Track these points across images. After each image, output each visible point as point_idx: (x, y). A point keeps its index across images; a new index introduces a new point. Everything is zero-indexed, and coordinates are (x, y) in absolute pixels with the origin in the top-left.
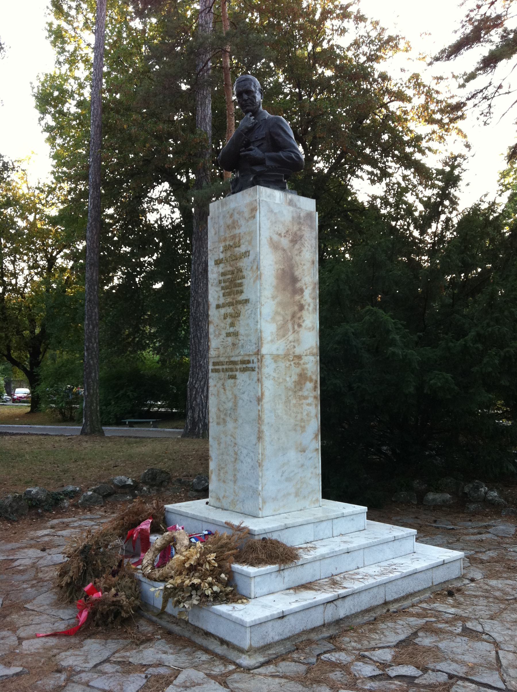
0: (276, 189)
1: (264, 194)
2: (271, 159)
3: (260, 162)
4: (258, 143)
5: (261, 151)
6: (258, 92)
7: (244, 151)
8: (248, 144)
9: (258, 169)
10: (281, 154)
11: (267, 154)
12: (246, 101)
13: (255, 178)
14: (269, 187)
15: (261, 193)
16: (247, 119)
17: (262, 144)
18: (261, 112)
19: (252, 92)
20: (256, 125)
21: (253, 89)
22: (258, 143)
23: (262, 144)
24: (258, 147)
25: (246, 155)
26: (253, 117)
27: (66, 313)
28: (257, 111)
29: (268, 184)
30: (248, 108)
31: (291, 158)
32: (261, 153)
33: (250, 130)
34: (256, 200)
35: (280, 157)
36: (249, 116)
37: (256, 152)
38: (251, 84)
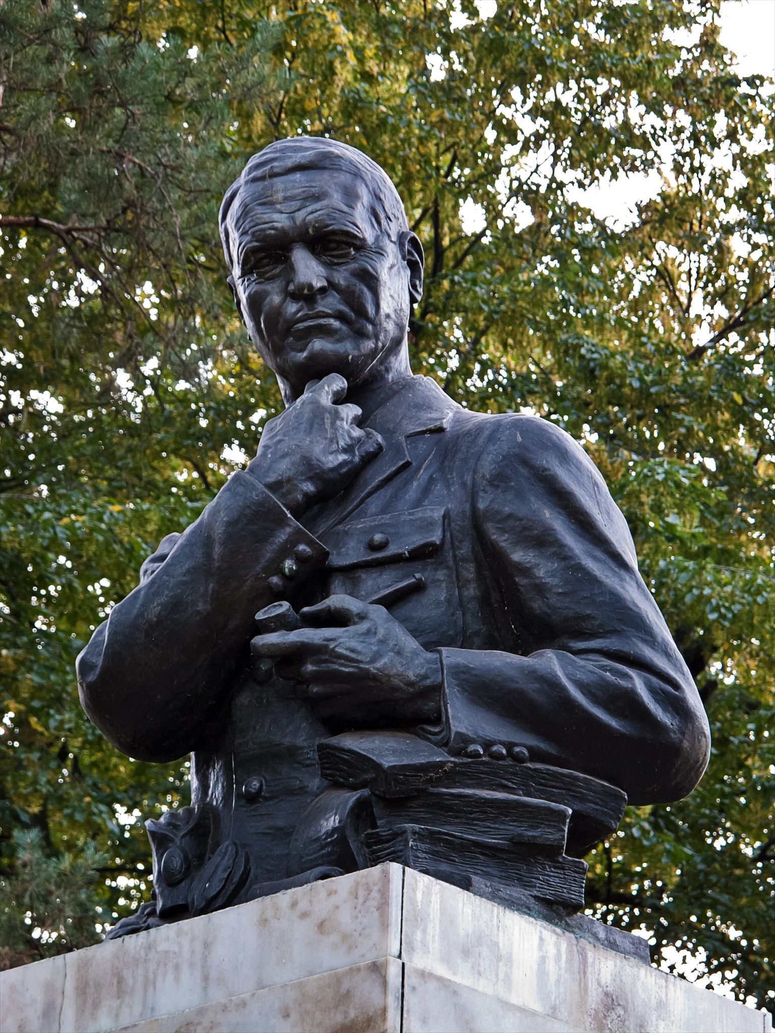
0: (511, 904)
1: (434, 929)
2: (488, 693)
3: (407, 709)
4: (388, 582)
5: (415, 633)
6: (391, 249)
7: (282, 623)
8: (313, 579)
9: (386, 750)
10: (551, 661)
11: (452, 656)
12: (307, 295)
13: (361, 814)
14: (465, 884)
15: (420, 919)
16: (318, 412)
17: (418, 588)
18: (406, 386)
19: (359, 245)
20: (370, 459)
21: (368, 233)
22: (388, 582)
23: (418, 588)
24: (391, 602)
25: (302, 652)
26: (351, 411)
27: (217, 27)
28: (377, 377)
29: (455, 863)
30: (317, 344)
31: (625, 703)
32: (411, 643)
33: (334, 492)
34: (377, 969)
35: (553, 684)
36: (326, 400)
37: (373, 638)
38: (351, 196)
